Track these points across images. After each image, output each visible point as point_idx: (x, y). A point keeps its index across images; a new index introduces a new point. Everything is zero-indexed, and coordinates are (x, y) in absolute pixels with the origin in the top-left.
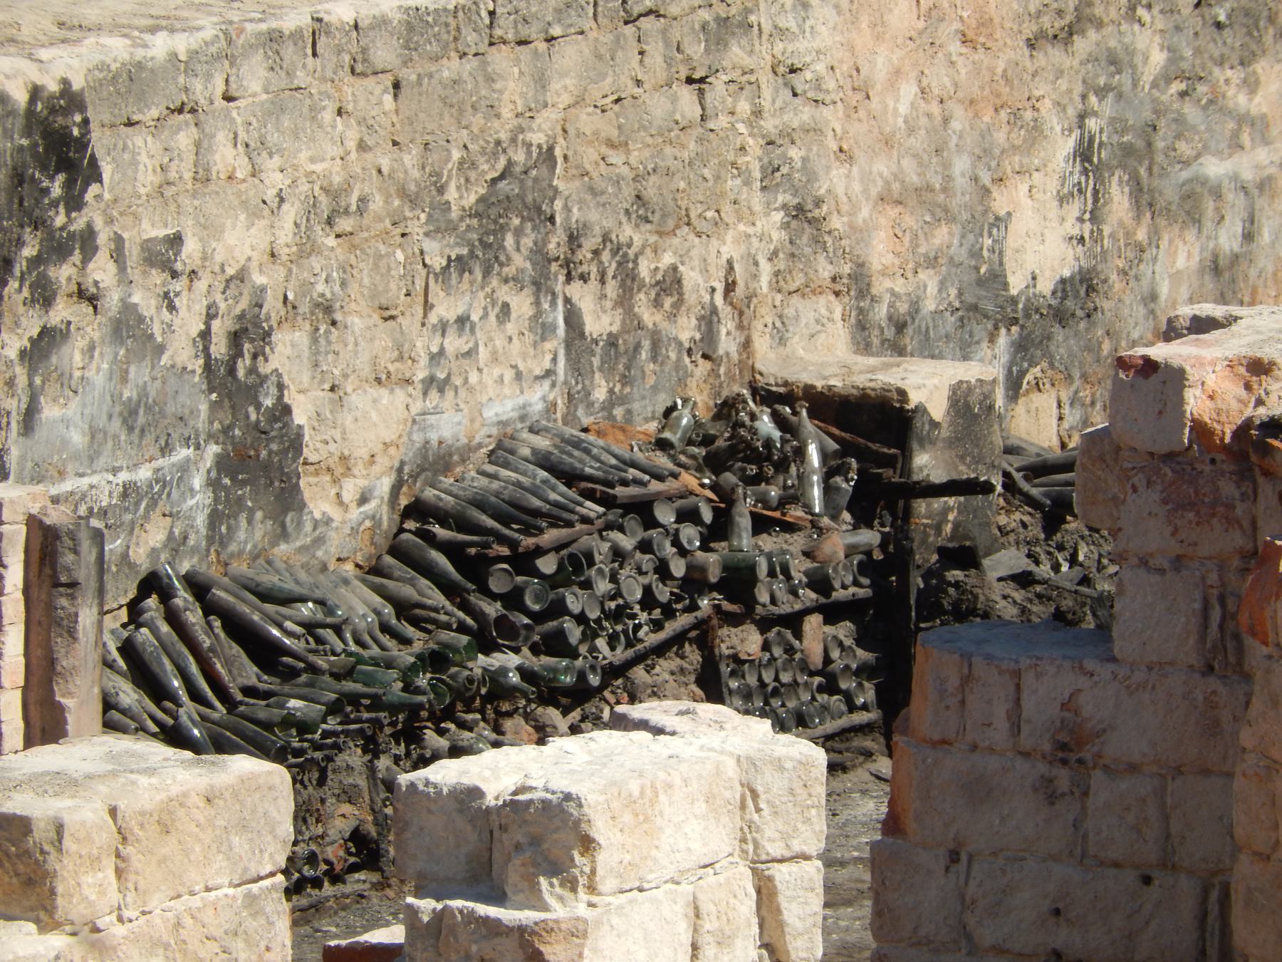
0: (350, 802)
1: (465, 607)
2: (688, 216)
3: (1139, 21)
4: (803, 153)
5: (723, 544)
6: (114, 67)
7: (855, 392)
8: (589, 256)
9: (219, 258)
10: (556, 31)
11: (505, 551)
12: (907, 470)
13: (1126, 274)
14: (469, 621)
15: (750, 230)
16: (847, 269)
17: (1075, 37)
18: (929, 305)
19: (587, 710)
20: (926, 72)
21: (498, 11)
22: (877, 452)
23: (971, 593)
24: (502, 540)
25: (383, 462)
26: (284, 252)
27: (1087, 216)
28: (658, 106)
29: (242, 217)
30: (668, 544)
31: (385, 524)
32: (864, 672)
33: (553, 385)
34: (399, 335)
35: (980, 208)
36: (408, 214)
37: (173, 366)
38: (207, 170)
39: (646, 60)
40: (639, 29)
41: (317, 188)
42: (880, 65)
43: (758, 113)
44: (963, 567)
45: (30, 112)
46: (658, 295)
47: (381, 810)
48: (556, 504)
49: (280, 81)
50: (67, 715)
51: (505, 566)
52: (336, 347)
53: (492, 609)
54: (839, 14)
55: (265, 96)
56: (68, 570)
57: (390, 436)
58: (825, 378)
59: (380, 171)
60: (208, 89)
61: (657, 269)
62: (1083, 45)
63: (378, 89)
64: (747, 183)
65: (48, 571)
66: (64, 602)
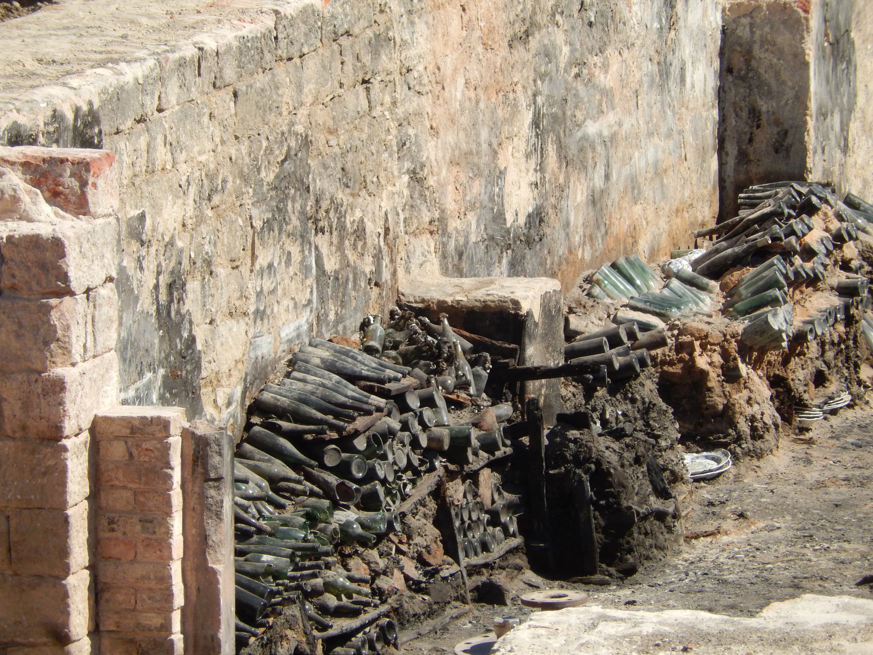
0: (290, 628)
1: (309, 478)
2: (365, 181)
3: (557, 24)
4: (414, 131)
6: (111, 90)
7: (478, 304)
8: (324, 214)
9: (161, 229)
10: (305, 50)
11: (335, 435)
12: (522, 360)
13: (556, 208)
14: (316, 489)
15: (394, 189)
16: (437, 215)
17: (530, 38)
18: (473, 238)
19: (381, 549)
20: (468, 68)
21: (280, 36)
22: (500, 347)
23: (586, 446)
24: (332, 427)
25: (237, 376)
26: (189, 222)
27: (538, 168)
29: (170, 198)
30: (416, 423)
31: (239, 422)
32: (510, 507)
33: (311, 311)
34: (240, 280)
35: (493, 165)
36: (244, 190)
37: (142, 312)
38: (154, 164)
39: (344, 67)
40: (340, 45)
41: (203, 174)
42: (448, 65)
43: (394, 103)
44: (578, 428)
45: (75, 127)
46: (355, 240)
47: (311, 633)
48: (353, 398)
49: (185, 98)
50: (219, 577)
51: (334, 446)
52: (213, 291)
53: (333, 480)
54: (428, 28)
55: (177, 108)
56: (216, 468)
57: (238, 355)
58: (451, 295)
59: (231, 159)
61: (354, 221)
62: (534, 43)
63: (226, 95)
64: (391, 155)
65: (200, 470)
66: (212, 492)
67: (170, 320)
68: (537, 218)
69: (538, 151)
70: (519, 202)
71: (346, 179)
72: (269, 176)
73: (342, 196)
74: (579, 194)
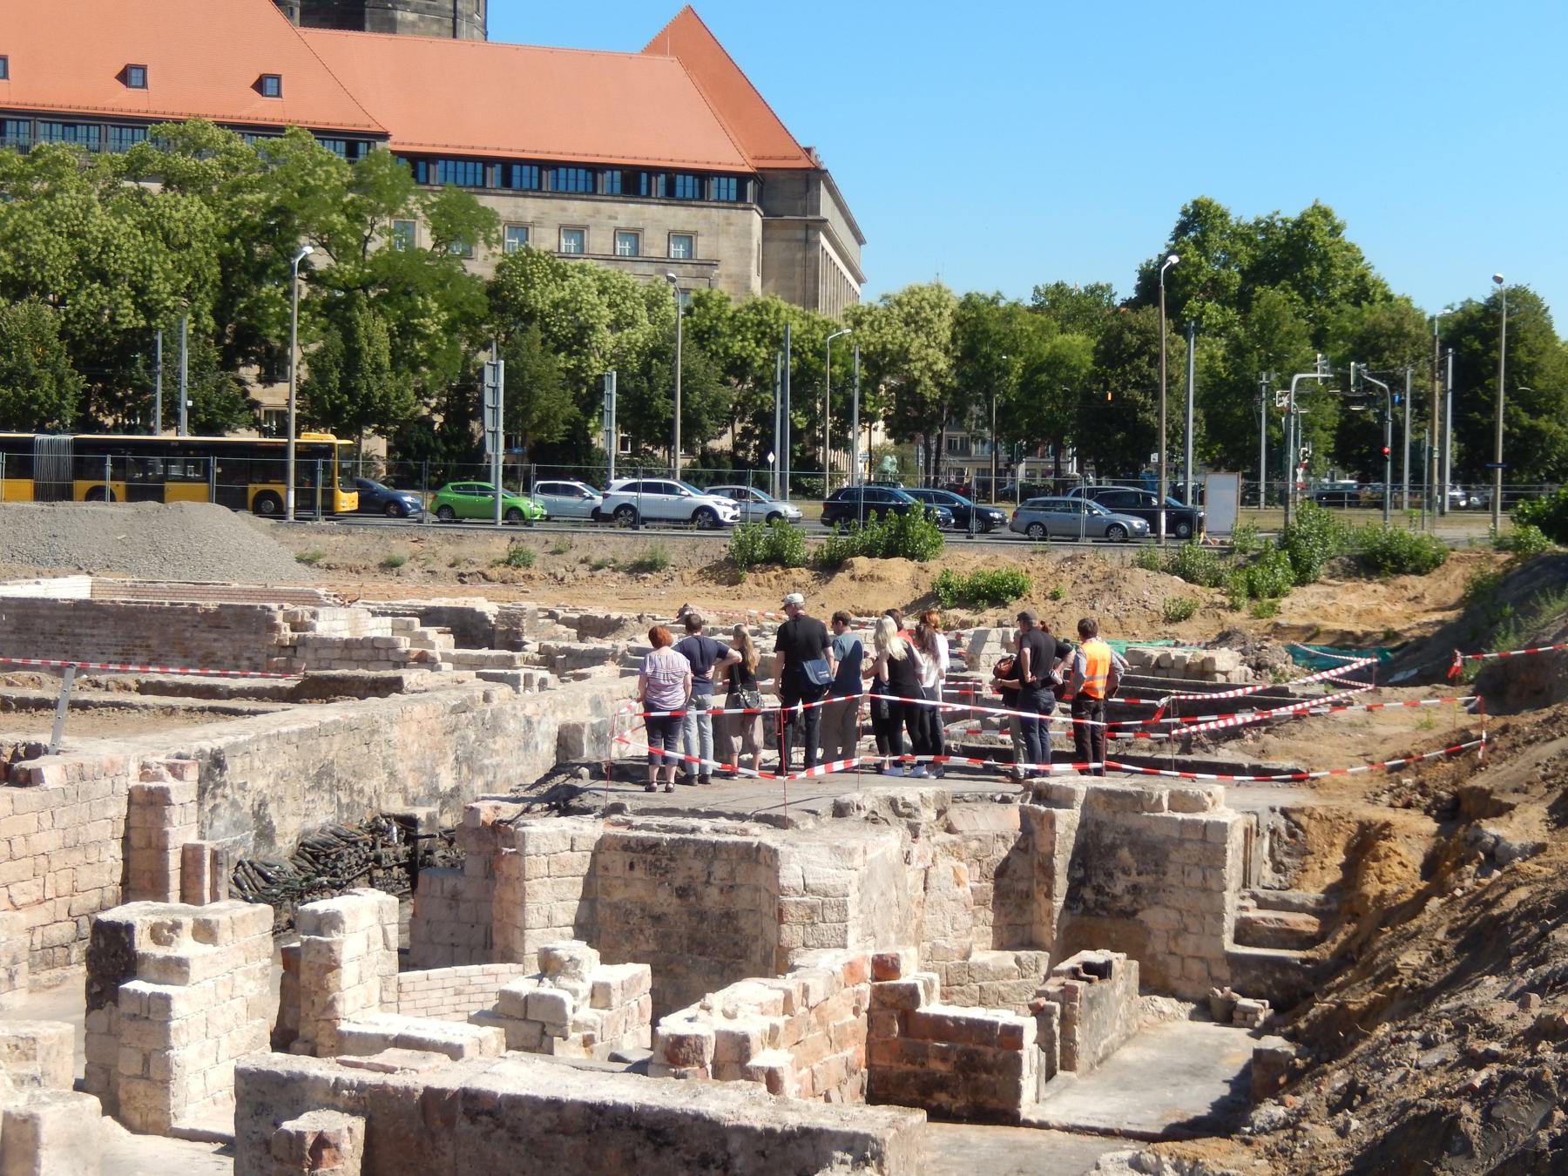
28: (358, 750)
60: (252, 748)
71: (354, 774)
72: (312, 772)
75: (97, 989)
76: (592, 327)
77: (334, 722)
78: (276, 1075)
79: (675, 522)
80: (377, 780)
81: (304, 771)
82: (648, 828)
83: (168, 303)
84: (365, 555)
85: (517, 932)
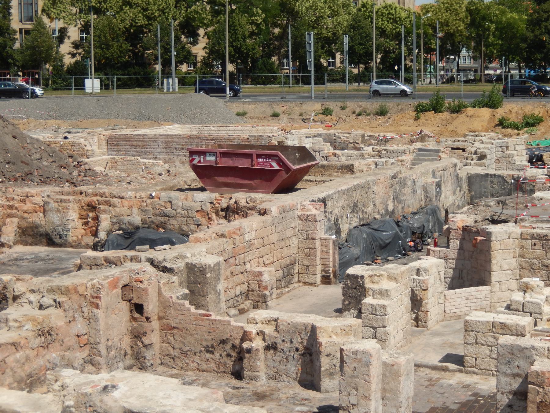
5: (156, 318)
12: (211, 6)
28: (364, 195)
60: (334, 196)
62: (393, 188)
67: (336, 224)
68: (393, 210)
69: (394, 201)
70: (391, 208)
71: (364, 206)
73: (363, 208)
74: (400, 207)
75: (347, 302)
76: (322, 17)
77: (357, 184)
78: (519, 346)
79: (395, 95)
80: (369, 209)
81: (349, 205)
82: (542, 228)
83: (156, 14)
84: (264, 112)
85: (487, 273)
